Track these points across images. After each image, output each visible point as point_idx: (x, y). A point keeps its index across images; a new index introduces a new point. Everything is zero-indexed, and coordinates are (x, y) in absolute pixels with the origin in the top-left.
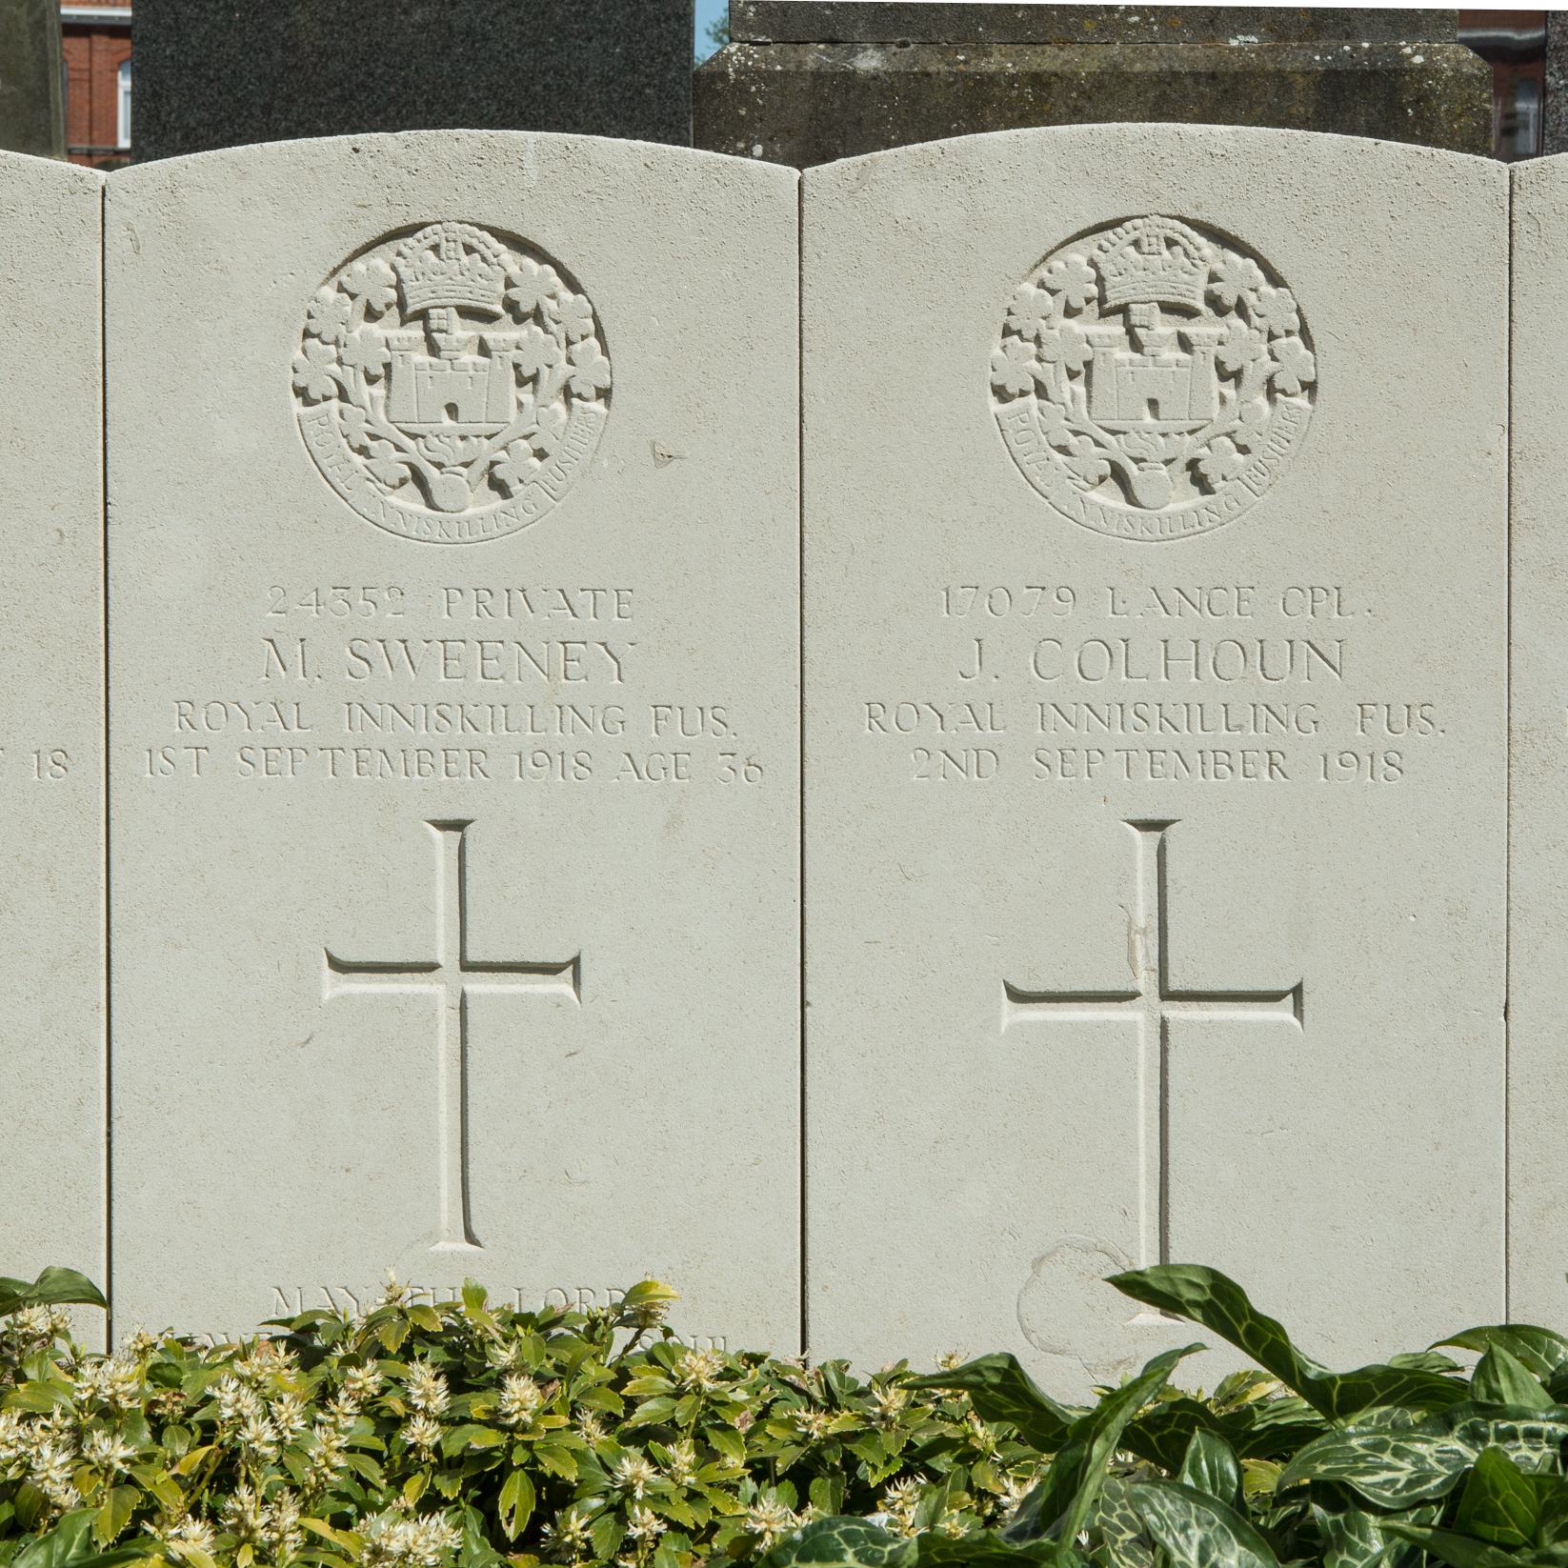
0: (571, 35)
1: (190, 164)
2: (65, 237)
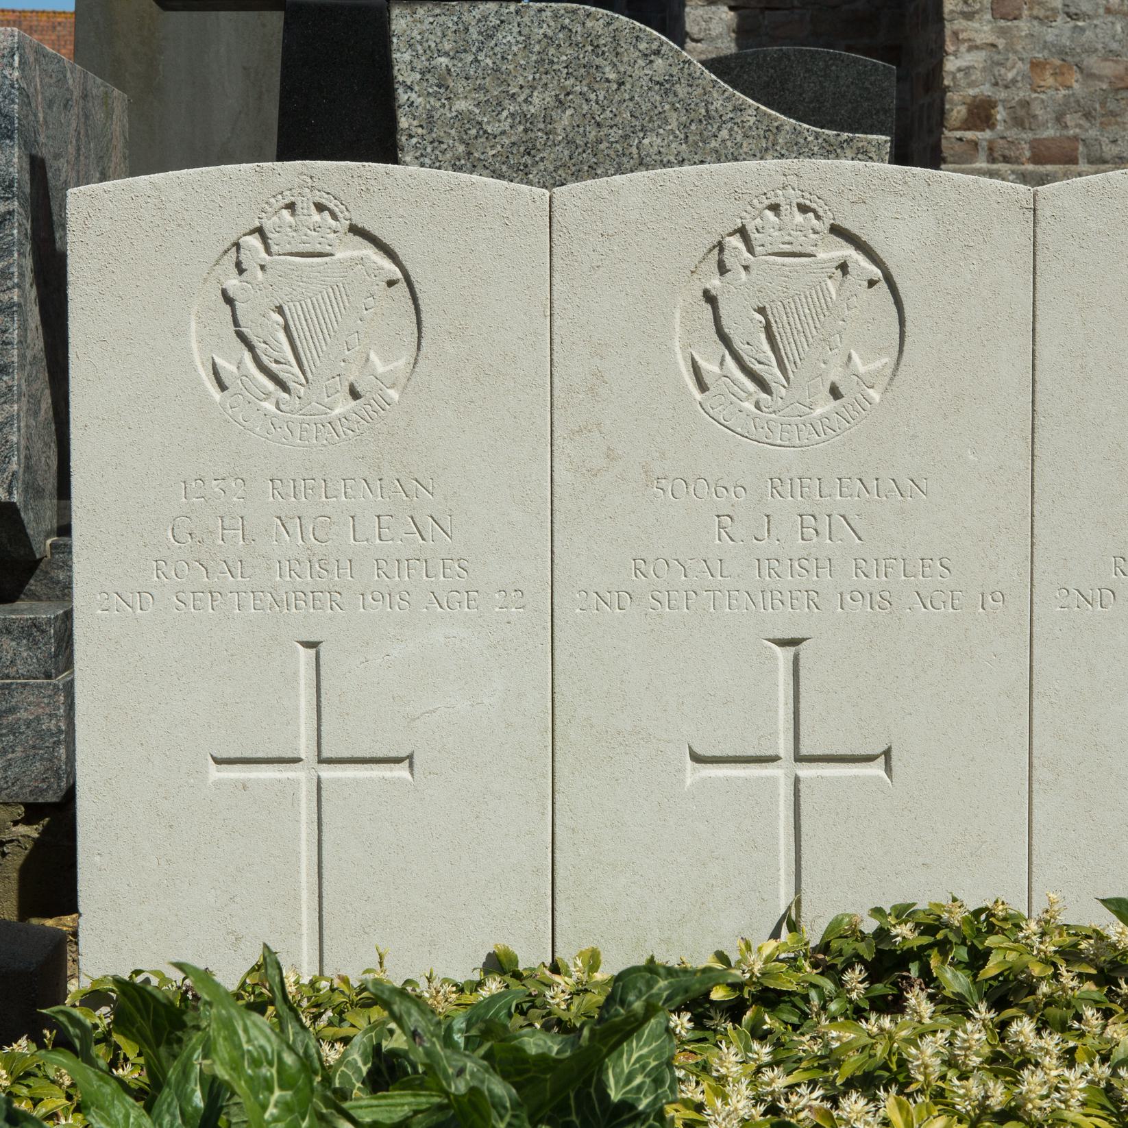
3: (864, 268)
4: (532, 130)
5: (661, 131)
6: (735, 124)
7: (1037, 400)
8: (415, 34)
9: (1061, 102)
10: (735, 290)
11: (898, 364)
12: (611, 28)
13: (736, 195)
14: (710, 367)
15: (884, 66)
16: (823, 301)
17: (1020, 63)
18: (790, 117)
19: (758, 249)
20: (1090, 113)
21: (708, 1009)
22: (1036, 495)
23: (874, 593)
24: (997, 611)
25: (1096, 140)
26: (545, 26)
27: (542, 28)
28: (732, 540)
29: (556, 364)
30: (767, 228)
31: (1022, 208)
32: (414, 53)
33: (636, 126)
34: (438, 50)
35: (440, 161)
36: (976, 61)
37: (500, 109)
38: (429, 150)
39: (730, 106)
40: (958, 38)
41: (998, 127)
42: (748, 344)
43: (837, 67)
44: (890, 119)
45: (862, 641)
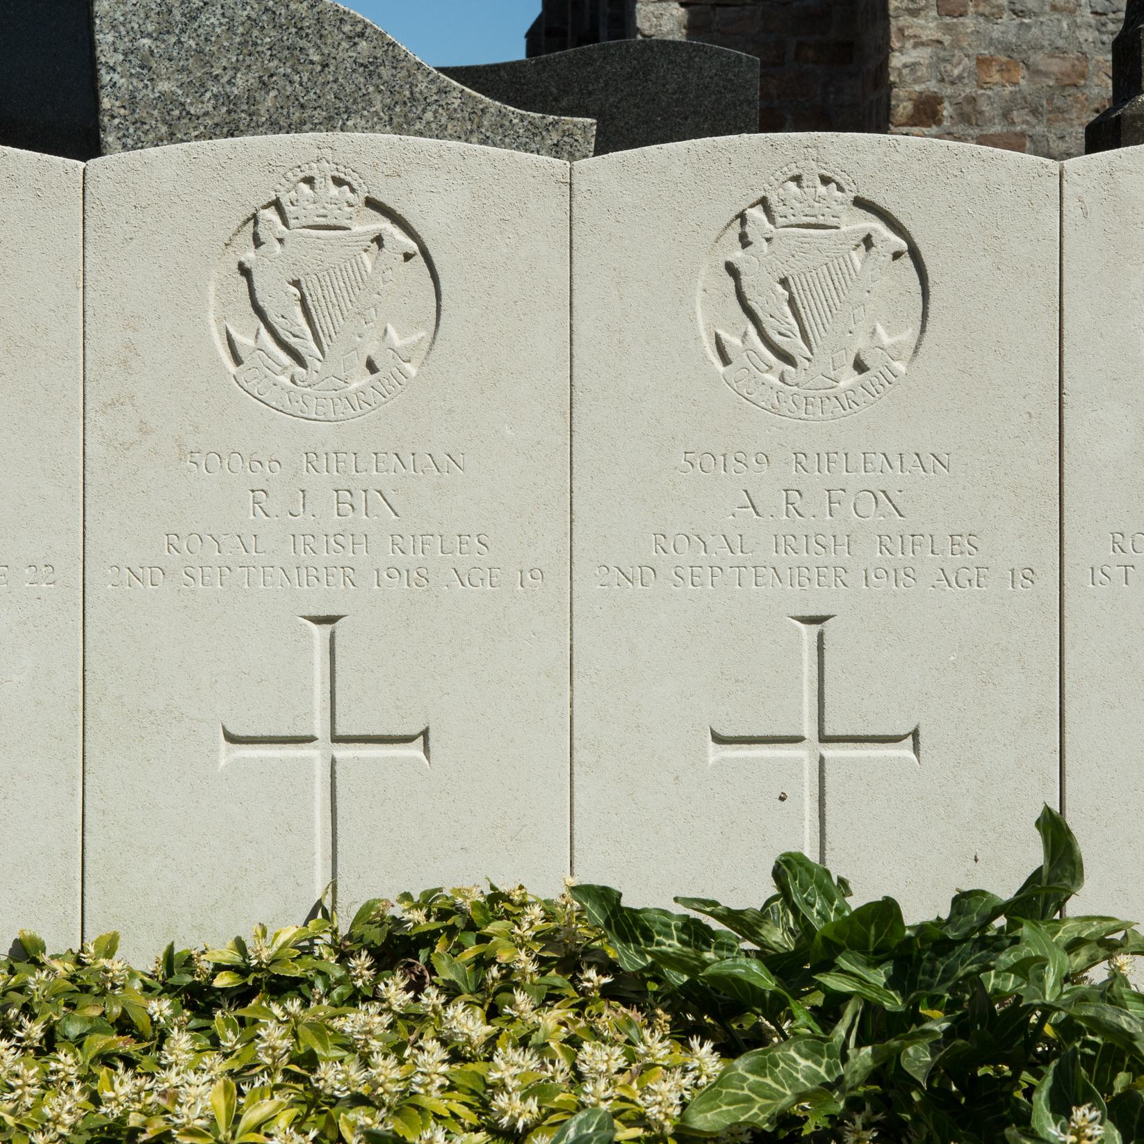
0: (674, 116)
1: (1123, 155)
2: (1035, 206)
3: (399, 242)
4: (235, 112)
5: (365, 113)
6: (439, 106)
7: (575, 374)
8: (118, 14)
9: (1008, 99)
10: (269, 263)
11: (434, 338)
12: (315, 10)
13: (270, 168)
14: (244, 341)
15: (748, 57)
16: (358, 274)
17: (966, 59)
18: (496, 100)
19: (292, 222)
20: (1037, 109)
21: (218, 998)
22: (574, 471)
23: (411, 570)
24: (536, 589)
25: (1043, 136)
26: (248, 8)
27: (245, 10)
28: (267, 515)
29: (88, 336)
30: (301, 201)
31: (557, 182)
32: (117, 35)
33: (340, 107)
34: (141, 31)
35: (143, 142)
36: (922, 57)
37: (203, 90)
38: (131, 130)
39: (434, 88)
40: (903, 35)
41: (945, 123)
42: (283, 317)
43: (700, 58)
44: (754, 111)
45: (399, 619)
